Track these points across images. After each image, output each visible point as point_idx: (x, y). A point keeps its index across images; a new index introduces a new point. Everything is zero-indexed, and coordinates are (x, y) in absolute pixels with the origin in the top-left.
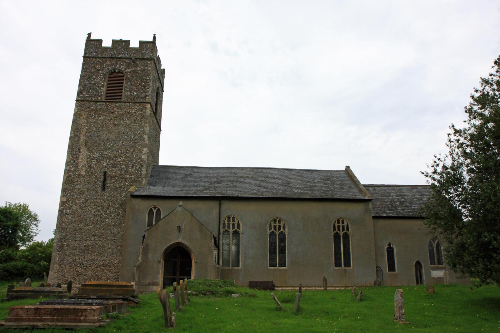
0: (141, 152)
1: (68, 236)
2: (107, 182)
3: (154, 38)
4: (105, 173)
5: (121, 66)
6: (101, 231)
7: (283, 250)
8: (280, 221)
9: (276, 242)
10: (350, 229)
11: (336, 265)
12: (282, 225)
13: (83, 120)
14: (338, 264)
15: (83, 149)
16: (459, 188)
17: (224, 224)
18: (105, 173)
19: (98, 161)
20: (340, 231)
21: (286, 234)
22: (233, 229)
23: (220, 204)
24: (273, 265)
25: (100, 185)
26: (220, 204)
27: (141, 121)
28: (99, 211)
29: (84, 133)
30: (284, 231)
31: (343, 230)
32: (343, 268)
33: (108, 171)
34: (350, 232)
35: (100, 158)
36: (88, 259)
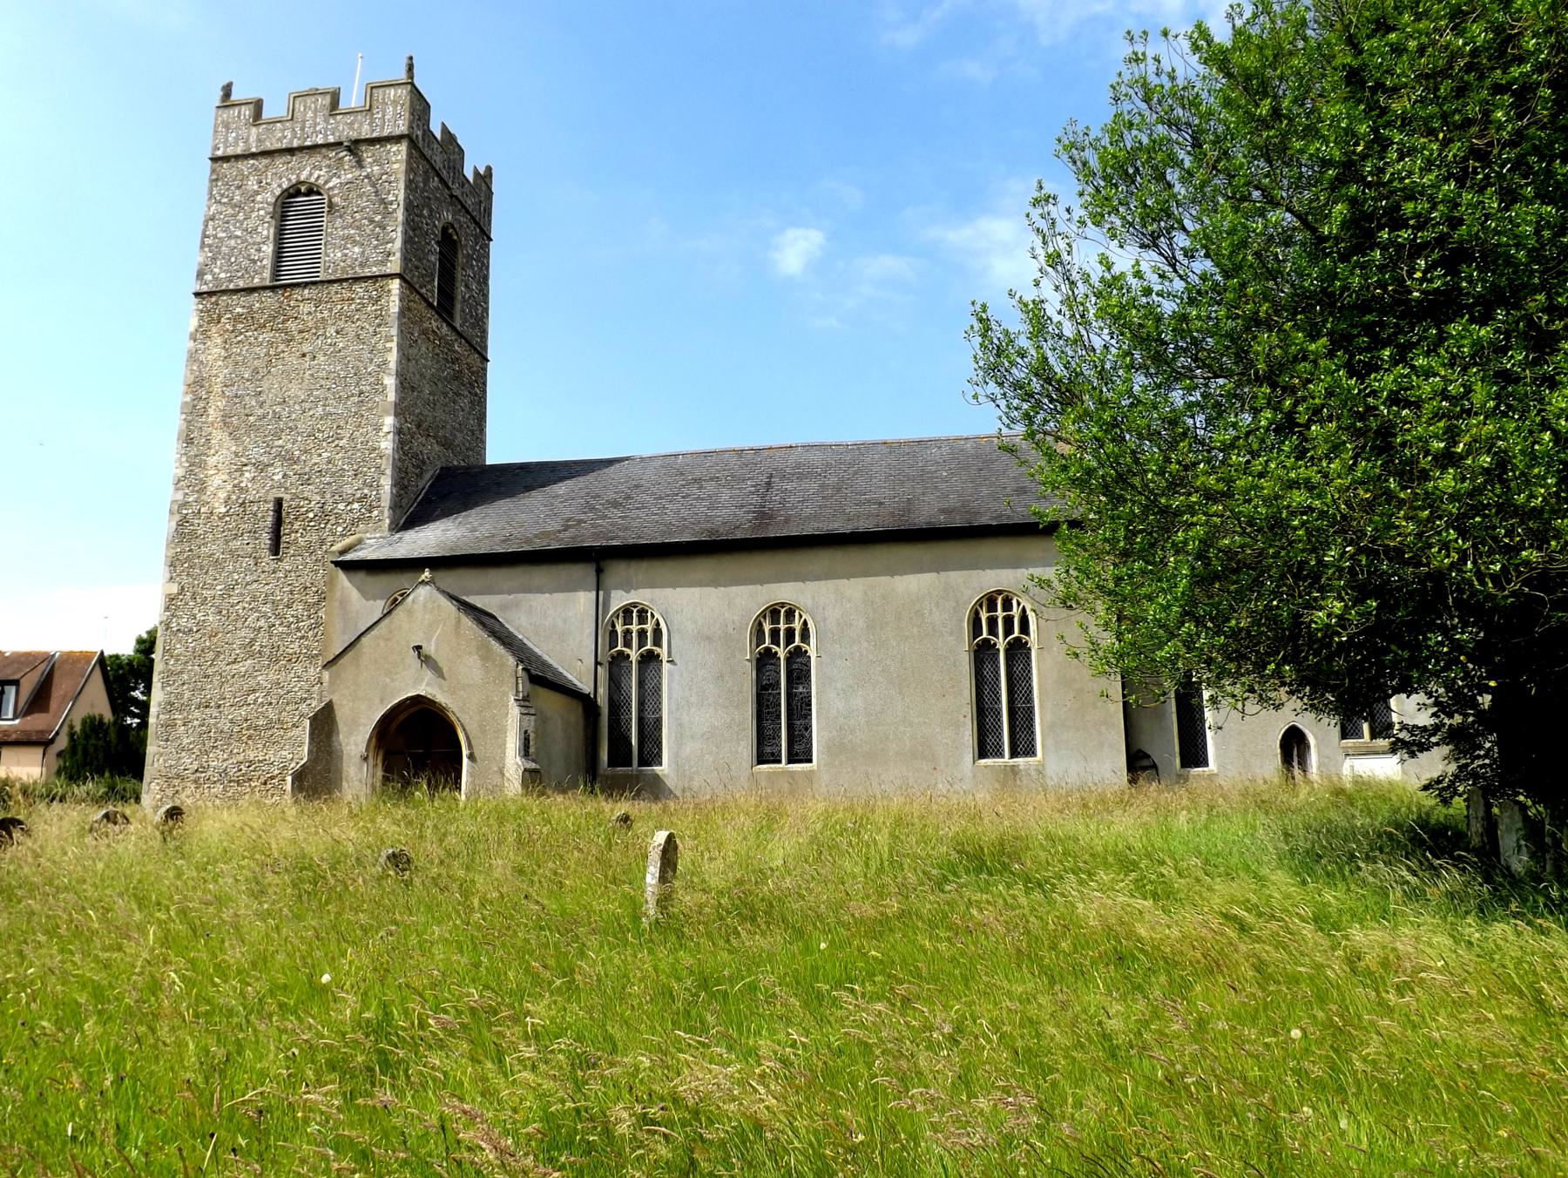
0: (378, 429)
1: (187, 695)
2: (285, 529)
3: (410, 68)
4: (279, 503)
5: (308, 171)
6: (272, 676)
7: (800, 709)
8: (790, 614)
9: (778, 683)
10: (1033, 627)
11: (983, 752)
12: (797, 625)
13: (215, 350)
14: (985, 749)
15: (218, 436)
16: (1086, 278)
17: (613, 633)
18: (279, 503)
19: (262, 467)
20: (996, 636)
21: (812, 653)
22: (1006, 636)
23: (599, 571)
24: (765, 755)
25: (266, 539)
26: (599, 571)
27: (375, 333)
28: (265, 616)
29: (217, 389)
30: (657, 650)
31: (1008, 630)
32: (1007, 759)
33: (287, 497)
34: (1033, 639)
35: (265, 459)
36: (241, 758)
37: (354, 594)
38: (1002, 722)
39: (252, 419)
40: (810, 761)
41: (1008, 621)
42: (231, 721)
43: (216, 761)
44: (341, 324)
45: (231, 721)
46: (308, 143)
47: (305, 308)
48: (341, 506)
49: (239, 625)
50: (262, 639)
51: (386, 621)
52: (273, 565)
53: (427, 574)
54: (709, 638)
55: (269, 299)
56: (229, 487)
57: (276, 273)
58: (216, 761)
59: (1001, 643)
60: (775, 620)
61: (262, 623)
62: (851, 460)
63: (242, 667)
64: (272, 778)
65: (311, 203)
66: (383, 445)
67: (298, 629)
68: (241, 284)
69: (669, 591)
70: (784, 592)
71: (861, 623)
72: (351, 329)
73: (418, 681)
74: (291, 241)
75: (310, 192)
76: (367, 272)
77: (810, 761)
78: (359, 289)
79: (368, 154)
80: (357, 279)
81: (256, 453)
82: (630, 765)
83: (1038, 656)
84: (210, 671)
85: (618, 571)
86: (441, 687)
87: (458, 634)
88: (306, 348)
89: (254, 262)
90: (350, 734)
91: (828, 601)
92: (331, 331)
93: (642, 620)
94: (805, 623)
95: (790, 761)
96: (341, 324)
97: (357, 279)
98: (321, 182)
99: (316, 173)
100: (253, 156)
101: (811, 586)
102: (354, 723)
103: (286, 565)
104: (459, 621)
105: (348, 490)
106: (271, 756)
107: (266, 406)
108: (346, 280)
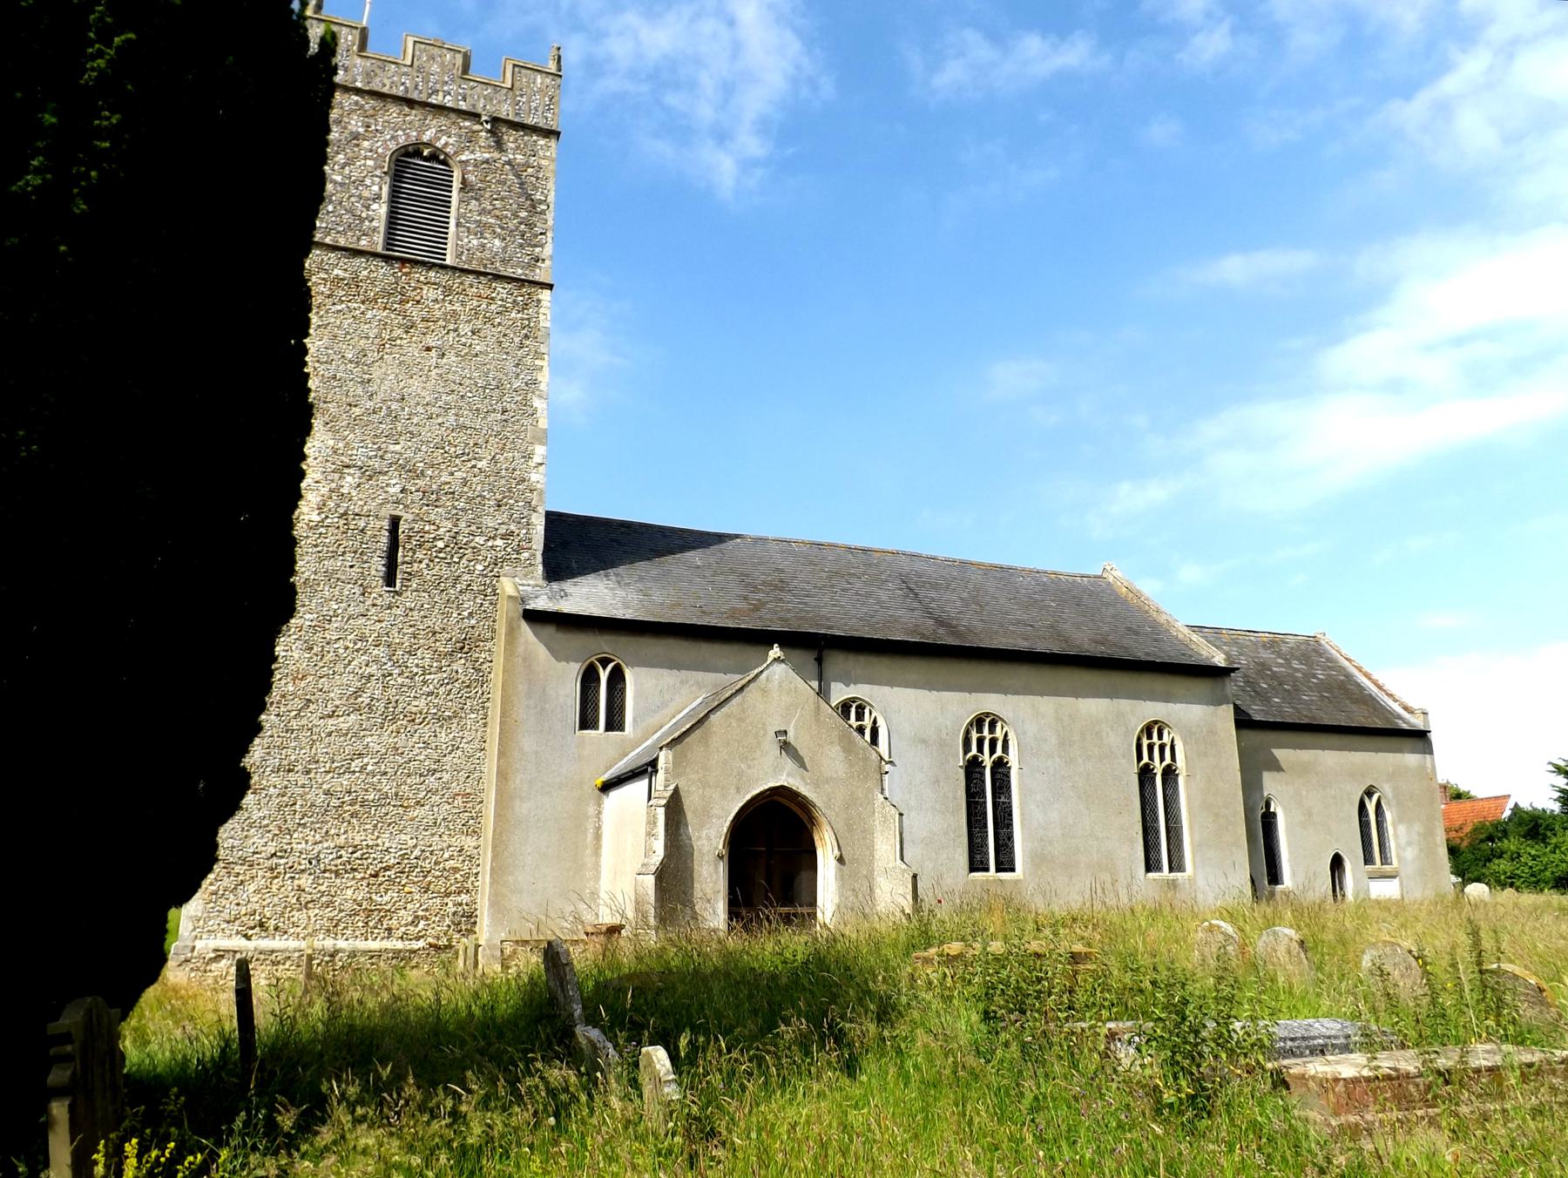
5: (432, 132)
18: (395, 522)
19: (370, 474)
25: (378, 565)
31: (993, 750)
33: (406, 516)
35: (376, 463)
36: (341, 840)
37: (542, 652)
38: (1159, 842)
39: (357, 411)
40: (1013, 870)
41: (993, 743)
42: (327, 793)
43: (303, 842)
44: (479, 323)
45: (327, 793)
46: (433, 100)
47: (430, 293)
48: (480, 540)
49: (339, 668)
50: (374, 688)
51: (738, 698)
52: (388, 599)
53: (776, 652)
54: (924, 742)
55: (382, 270)
56: (324, 491)
57: (390, 242)
58: (303, 842)
59: (1158, 769)
60: (980, 730)
61: (373, 669)
62: (862, 564)
63: (344, 723)
64: (386, 869)
65: (432, 170)
66: (534, 477)
67: (425, 682)
68: (342, 242)
69: (886, 689)
70: (990, 702)
71: (1054, 740)
72: (487, 330)
73: (777, 770)
74: (408, 210)
75: (433, 157)
76: (509, 272)
77: (1013, 870)
78: (501, 289)
79: (510, 138)
80: (498, 277)
81: (360, 455)
82: (987, 870)
83: (1187, 783)
84: (294, 724)
85: (837, 662)
86: (803, 779)
87: (817, 720)
88: (430, 341)
89: (362, 220)
90: (702, 826)
91: (1032, 720)
92: (465, 329)
93: (860, 717)
94: (875, 722)
95: (998, 870)
96: (479, 323)
97: (498, 277)
98: (449, 150)
99: (444, 139)
100: (358, 91)
101: (1012, 699)
102: (706, 813)
103: (408, 599)
104: (818, 708)
105: (489, 522)
106: (385, 840)
107: (377, 398)
108: (485, 274)
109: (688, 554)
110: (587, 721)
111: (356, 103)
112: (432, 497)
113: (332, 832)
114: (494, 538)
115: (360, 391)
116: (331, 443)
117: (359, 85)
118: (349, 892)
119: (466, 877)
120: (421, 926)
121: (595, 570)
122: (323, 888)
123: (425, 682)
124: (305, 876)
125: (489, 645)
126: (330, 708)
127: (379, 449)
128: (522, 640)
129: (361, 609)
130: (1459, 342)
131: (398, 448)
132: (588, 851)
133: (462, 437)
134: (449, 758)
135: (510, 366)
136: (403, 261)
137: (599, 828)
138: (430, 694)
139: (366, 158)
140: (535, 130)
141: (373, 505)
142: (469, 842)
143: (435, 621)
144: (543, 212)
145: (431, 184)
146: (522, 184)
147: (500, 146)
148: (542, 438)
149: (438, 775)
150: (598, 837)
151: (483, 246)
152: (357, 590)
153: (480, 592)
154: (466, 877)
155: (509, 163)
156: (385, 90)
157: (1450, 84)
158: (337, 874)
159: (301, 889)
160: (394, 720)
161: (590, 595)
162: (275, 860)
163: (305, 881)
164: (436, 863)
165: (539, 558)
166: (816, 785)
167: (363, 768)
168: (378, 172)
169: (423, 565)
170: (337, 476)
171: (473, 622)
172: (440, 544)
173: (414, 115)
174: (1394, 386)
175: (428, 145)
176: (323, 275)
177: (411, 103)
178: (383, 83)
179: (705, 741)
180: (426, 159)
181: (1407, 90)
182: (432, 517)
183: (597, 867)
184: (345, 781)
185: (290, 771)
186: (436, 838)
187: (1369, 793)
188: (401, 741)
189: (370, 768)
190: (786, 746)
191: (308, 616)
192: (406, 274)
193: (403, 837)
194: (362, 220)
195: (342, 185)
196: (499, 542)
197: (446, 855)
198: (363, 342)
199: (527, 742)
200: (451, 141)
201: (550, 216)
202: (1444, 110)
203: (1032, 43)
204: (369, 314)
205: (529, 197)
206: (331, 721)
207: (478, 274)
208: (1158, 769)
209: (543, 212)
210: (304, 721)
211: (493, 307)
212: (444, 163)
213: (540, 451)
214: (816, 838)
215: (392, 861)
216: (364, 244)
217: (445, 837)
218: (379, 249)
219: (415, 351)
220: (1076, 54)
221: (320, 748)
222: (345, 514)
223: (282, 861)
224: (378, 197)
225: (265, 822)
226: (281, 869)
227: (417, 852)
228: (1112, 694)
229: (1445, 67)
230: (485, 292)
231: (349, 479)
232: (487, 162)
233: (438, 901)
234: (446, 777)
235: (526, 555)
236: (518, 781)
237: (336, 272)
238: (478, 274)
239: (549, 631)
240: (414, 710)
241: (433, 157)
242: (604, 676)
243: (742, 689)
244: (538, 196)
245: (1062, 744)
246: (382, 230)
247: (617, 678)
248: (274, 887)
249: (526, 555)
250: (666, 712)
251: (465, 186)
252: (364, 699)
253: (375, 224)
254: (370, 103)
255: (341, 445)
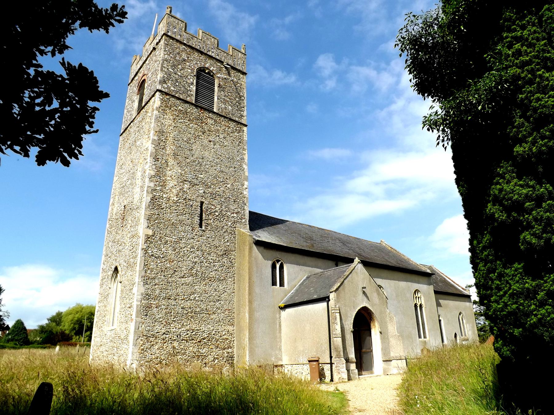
25: (197, 219)
35: (195, 181)
36: (188, 327)
37: (260, 256)
39: (188, 160)
42: (183, 308)
45: (183, 308)
47: (210, 121)
49: (185, 258)
50: (198, 267)
56: (178, 189)
64: (204, 339)
66: (245, 193)
68: (181, 97)
71: (394, 295)
73: (363, 301)
78: (232, 125)
79: (232, 72)
80: (231, 120)
81: (189, 177)
89: (188, 91)
97: (231, 120)
100: (185, 44)
106: (203, 328)
107: (195, 156)
109: (279, 225)
110: (274, 283)
111: (184, 49)
112: (214, 196)
113: (185, 324)
114: (233, 213)
115: (189, 153)
116: (180, 171)
117: (185, 42)
118: (191, 348)
119: (230, 342)
120: (216, 362)
121: (260, 229)
122: (182, 347)
123: (214, 266)
124: (176, 342)
125: (234, 253)
126: (183, 274)
127: (196, 176)
128: (254, 251)
129: (192, 236)
130: (385, 183)
131: (202, 176)
132: (278, 332)
133: (222, 175)
134: (223, 295)
135: (235, 151)
136: (202, 108)
137: (280, 323)
138: (216, 270)
139: (188, 69)
140: (239, 71)
141: (194, 197)
142: (230, 328)
143: (216, 243)
144: (243, 100)
145: (208, 83)
146: (237, 89)
147: (229, 74)
148: (246, 179)
149: (219, 302)
150: (280, 326)
151: (226, 108)
152: (190, 228)
153: (230, 233)
154: (230, 342)
155: (232, 80)
156: (193, 46)
157: (394, 107)
158: (187, 341)
159: (174, 348)
160: (204, 280)
161: (264, 236)
162: (165, 336)
163: (176, 344)
164: (221, 336)
165: (248, 223)
166: (373, 306)
167: (195, 298)
168: (192, 75)
169: (212, 221)
170: (182, 184)
171: (228, 244)
172: (217, 214)
173: (203, 57)
174: (367, 194)
175: (207, 68)
176: (175, 108)
177: (202, 53)
178: (193, 43)
179: (344, 289)
180: (206, 73)
181: (382, 108)
182: (214, 203)
183: (280, 336)
184: (188, 304)
185: (169, 299)
186: (220, 326)
187: (460, 314)
188: (207, 288)
189: (197, 298)
190: (364, 292)
191: (174, 237)
192: (202, 113)
193: (209, 326)
194: (188, 91)
195: (181, 76)
196: (235, 215)
197: (224, 333)
198: (189, 135)
199: (257, 290)
200: (214, 69)
201: (245, 101)
202: (390, 114)
203: (278, 74)
204: (191, 125)
205: (239, 94)
206: (183, 279)
207: (225, 117)
208: (418, 306)
209: (243, 100)
210: (173, 279)
211: (230, 130)
212: (212, 76)
213: (246, 183)
214: (372, 325)
215: (206, 336)
216: (188, 99)
217: (223, 326)
218: (194, 102)
219: (206, 142)
220: (292, 79)
221: (179, 290)
222: (185, 199)
223: (167, 336)
224: (192, 84)
225: (161, 320)
226: (167, 339)
227: (214, 332)
228: (406, 281)
229: (392, 102)
230: (227, 124)
231: (186, 185)
232: (225, 79)
233: (221, 351)
234: (222, 302)
235: (244, 220)
236: (255, 304)
237: (179, 108)
238: (225, 117)
239: (262, 248)
240: (211, 276)
241: (209, 73)
242: (278, 266)
243: (351, 272)
244: (241, 94)
245: (397, 296)
246: (194, 95)
247: (281, 267)
248: (165, 347)
249: (244, 220)
250: (297, 280)
251: (219, 86)
252: (194, 271)
253: (192, 93)
254: (189, 50)
255: (183, 172)
